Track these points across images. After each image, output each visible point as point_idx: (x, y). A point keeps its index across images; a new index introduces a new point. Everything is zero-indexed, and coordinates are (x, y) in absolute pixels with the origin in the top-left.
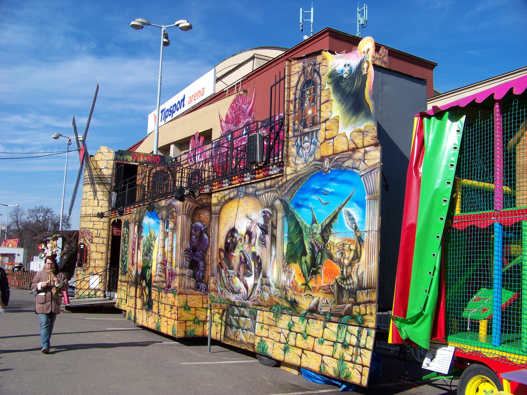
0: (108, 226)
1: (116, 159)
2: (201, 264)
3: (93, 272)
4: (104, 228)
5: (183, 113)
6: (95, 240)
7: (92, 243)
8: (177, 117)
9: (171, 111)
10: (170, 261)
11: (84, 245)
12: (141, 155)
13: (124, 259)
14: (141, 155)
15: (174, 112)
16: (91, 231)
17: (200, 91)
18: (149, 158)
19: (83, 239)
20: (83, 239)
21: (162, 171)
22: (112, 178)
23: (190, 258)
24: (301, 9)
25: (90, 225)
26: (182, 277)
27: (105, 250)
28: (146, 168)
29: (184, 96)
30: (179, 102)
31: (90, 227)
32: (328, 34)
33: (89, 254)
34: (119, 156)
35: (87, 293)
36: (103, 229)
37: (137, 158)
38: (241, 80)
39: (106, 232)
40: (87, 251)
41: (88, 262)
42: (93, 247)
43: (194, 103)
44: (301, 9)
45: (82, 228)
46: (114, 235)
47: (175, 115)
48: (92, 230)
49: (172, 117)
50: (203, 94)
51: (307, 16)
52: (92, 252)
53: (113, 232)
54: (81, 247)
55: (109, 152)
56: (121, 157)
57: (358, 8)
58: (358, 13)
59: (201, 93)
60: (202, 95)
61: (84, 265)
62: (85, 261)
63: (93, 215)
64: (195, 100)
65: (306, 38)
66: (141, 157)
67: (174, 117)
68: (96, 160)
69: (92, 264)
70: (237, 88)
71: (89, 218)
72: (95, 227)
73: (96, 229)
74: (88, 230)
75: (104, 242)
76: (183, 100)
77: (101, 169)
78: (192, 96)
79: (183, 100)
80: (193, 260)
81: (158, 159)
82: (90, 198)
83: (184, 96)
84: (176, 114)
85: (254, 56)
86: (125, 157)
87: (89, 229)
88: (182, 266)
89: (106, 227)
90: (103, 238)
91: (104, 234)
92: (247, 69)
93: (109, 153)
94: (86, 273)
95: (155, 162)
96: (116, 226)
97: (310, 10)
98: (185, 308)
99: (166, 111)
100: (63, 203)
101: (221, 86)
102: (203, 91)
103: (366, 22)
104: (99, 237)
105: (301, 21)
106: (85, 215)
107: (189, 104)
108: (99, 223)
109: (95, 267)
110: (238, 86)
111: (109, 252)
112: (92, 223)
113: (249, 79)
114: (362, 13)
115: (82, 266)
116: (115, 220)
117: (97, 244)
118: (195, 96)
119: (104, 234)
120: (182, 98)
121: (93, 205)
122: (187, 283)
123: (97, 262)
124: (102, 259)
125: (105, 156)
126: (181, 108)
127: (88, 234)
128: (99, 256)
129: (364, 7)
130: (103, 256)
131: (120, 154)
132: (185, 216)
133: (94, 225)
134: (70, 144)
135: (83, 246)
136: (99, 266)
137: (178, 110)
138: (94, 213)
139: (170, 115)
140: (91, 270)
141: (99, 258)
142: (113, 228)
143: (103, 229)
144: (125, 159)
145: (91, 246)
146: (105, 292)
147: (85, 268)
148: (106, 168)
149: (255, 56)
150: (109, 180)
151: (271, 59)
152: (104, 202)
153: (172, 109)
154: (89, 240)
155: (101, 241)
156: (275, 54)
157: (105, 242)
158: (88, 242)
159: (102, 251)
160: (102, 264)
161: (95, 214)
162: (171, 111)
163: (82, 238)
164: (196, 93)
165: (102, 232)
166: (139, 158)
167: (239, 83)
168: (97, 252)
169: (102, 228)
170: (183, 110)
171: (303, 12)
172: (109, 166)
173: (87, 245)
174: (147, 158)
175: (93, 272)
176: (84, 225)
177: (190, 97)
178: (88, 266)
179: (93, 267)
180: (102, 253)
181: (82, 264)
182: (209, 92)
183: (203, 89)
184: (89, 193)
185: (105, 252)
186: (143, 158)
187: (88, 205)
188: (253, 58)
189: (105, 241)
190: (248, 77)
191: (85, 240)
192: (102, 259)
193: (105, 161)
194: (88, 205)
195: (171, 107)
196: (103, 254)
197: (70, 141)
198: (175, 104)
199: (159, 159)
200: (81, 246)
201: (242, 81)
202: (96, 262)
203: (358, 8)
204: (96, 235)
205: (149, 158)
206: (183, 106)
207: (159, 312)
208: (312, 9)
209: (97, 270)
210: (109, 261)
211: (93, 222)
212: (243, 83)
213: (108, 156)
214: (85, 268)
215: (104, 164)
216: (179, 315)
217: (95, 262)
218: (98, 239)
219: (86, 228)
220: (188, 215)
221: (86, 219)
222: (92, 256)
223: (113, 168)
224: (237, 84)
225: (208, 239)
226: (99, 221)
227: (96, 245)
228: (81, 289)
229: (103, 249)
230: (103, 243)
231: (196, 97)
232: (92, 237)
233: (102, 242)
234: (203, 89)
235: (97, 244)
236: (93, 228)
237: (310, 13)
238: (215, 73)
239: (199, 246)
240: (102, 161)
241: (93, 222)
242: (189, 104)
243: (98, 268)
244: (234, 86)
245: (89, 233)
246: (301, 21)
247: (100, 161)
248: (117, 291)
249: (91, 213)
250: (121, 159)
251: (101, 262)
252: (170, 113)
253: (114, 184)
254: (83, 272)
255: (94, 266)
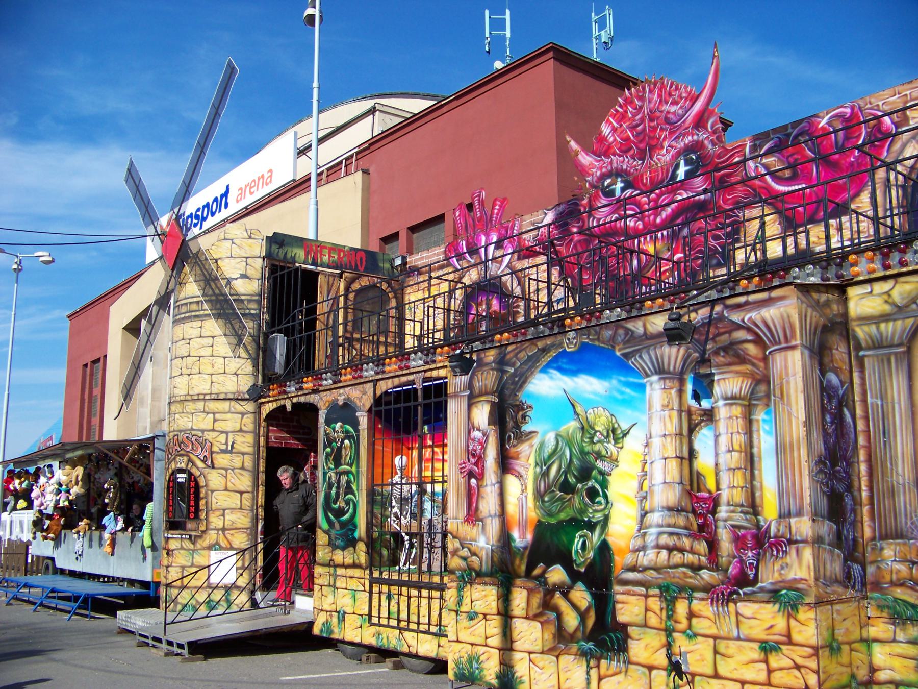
0: (255, 423)
1: (269, 256)
2: (848, 500)
3: (217, 543)
4: (244, 428)
5: (224, 220)
6: (221, 460)
7: (213, 467)
8: (208, 231)
9: (197, 217)
10: (739, 496)
11: (190, 474)
12: (326, 248)
13: (341, 504)
14: (326, 248)
15: (205, 219)
16: (210, 436)
17: (263, 176)
18: (342, 254)
19: (185, 459)
20: (185, 459)
21: (373, 286)
22: (259, 302)
23: (827, 483)
24: (487, 12)
25: (205, 422)
26: (819, 547)
27: (250, 484)
28: (337, 279)
29: (228, 187)
30: (216, 200)
31: (203, 427)
32: (551, 54)
33: (206, 497)
34: (275, 248)
35: (202, 596)
36: (241, 430)
37: (316, 254)
38: (356, 150)
39: (250, 438)
40: (197, 487)
41: (203, 516)
42: (214, 479)
43: (249, 200)
44: (487, 12)
45: (181, 431)
46: (271, 444)
47: (207, 225)
48: (211, 433)
49: (201, 228)
50: (271, 182)
51: (498, 25)
52: (212, 491)
53: (267, 438)
54: (179, 480)
55: (250, 237)
56: (281, 250)
57: (593, 14)
58: (593, 23)
59: (264, 179)
60: (267, 184)
61: (190, 525)
62: (192, 516)
63: (213, 396)
64: (251, 193)
65: (499, 65)
66: (326, 252)
67: (204, 228)
68: (216, 257)
69: (216, 521)
70: (346, 166)
71: (200, 405)
72: (219, 426)
73: (222, 432)
74: (200, 434)
75: (246, 464)
76: (226, 195)
77: (229, 281)
78: (246, 187)
79: (226, 195)
80: (832, 490)
81: (361, 260)
82: (202, 354)
83: (228, 187)
84: (210, 222)
85: (374, 108)
86: (290, 250)
87: (203, 431)
88: (816, 514)
89: (250, 427)
90: (243, 454)
91: (244, 443)
92: (362, 133)
93: (251, 241)
94: (198, 546)
95: (356, 266)
96: (274, 422)
97: (504, 14)
98: (830, 647)
99: (188, 217)
100: (6, 393)
101: (307, 166)
102: (271, 176)
103: (611, 39)
104: (231, 452)
105: (487, 35)
106: (189, 398)
107: (238, 201)
108: (229, 416)
109: (224, 529)
110: (348, 162)
111: (261, 489)
112: (211, 416)
113: (373, 148)
114: (602, 25)
115: (184, 529)
116: (284, 406)
117: (226, 470)
118: (251, 186)
119: (245, 443)
120: (223, 191)
121: (211, 372)
122: (828, 566)
123: (229, 517)
124: (241, 508)
125: (240, 247)
126: (220, 211)
127: (201, 444)
128: (234, 500)
129: (607, 12)
130: (244, 501)
131: (276, 243)
132: (806, 352)
133: (215, 420)
134: (20, 270)
135: (185, 476)
136: (235, 526)
137: (213, 214)
138: (214, 390)
139: (195, 225)
140: (211, 537)
141: (233, 506)
142: (268, 427)
143: (241, 430)
144: (289, 256)
145: (209, 477)
146: (253, 592)
147: (193, 533)
148: (244, 276)
149: (378, 107)
150: (253, 306)
151: (409, 116)
152: (243, 361)
153: (200, 213)
154: (204, 461)
155: (237, 461)
156: (417, 105)
157: (249, 463)
158: (200, 464)
159: (242, 489)
160: (244, 520)
161: (218, 394)
162: (197, 217)
163: (182, 455)
164: (254, 181)
165: (239, 439)
166: (321, 254)
167: (352, 156)
168: (226, 489)
169: (238, 428)
170: (224, 214)
171: (490, 18)
172: (250, 272)
173: (197, 473)
174: (339, 255)
175: (217, 543)
176: (183, 422)
177: (241, 189)
178: (203, 528)
179: (218, 530)
180: (241, 493)
181: (185, 523)
182: (282, 178)
183: (271, 171)
184: (199, 340)
185: (250, 489)
186: (330, 256)
187: (194, 371)
188: (372, 111)
189: (249, 462)
190: (371, 145)
191: (190, 460)
192: (241, 508)
193: (239, 260)
194: (195, 370)
195: (198, 210)
196: (245, 495)
197: (20, 264)
198: (208, 203)
199: (364, 259)
200: (179, 475)
201: (357, 153)
202: (227, 517)
203: (593, 14)
204: (224, 447)
205: (342, 254)
206: (226, 206)
207: (34, 604)
208: (508, 12)
209: (229, 537)
210: (261, 512)
211: (214, 414)
212: (359, 156)
213: (247, 248)
214: (193, 533)
215: (238, 266)
216: (823, 672)
217: (223, 515)
218: (228, 456)
219: (192, 429)
220: (811, 350)
221: (190, 407)
222: (214, 501)
223: (262, 278)
224: (347, 159)
225: (851, 423)
226: (229, 412)
227: (224, 472)
228: (184, 587)
229: (245, 482)
230: (243, 468)
231: (255, 188)
232: (212, 453)
233: (239, 465)
234: (271, 171)
235: (226, 470)
236: (213, 430)
237: (505, 19)
238: (296, 139)
239: (840, 448)
240: (232, 261)
241: (214, 414)
242: (238, 201)
243: (232, 532)
244: (341, 162)
245: (201, 443)
246: (487, 35)
247: (227, 260)
248: (311, 590)
249: (205, 392)
250: (281, 256)
251: (239, 515)
252: (195, 221)
253: (266, 317)
254: (187, 544)
255: (221, 526)
